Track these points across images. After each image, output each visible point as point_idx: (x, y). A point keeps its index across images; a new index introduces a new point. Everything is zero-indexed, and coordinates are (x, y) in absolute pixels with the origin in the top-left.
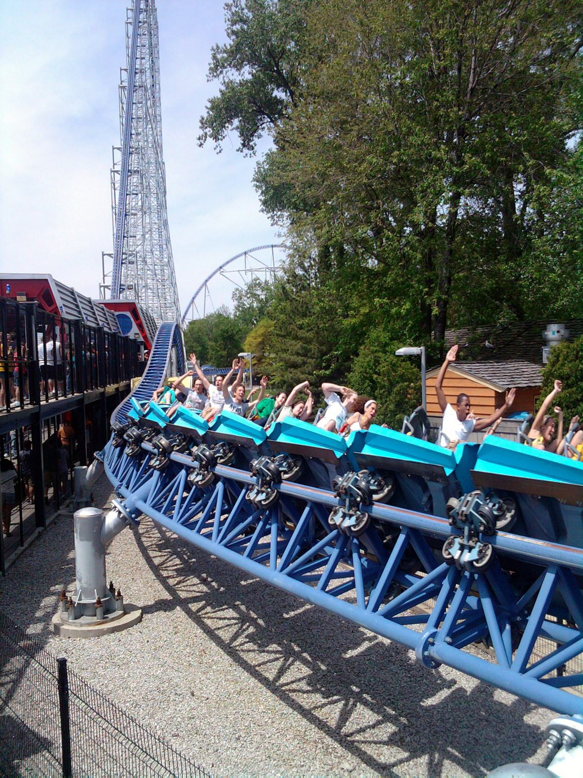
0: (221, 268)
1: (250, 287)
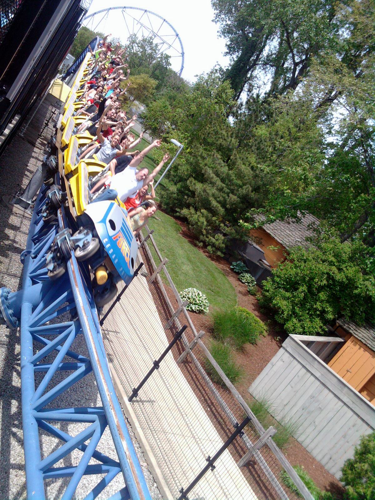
0: (125, 7)
1: (144, 40)
